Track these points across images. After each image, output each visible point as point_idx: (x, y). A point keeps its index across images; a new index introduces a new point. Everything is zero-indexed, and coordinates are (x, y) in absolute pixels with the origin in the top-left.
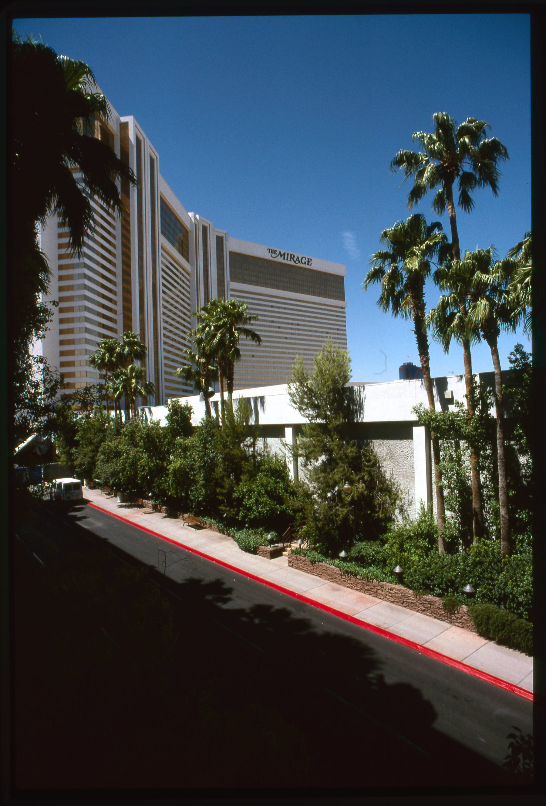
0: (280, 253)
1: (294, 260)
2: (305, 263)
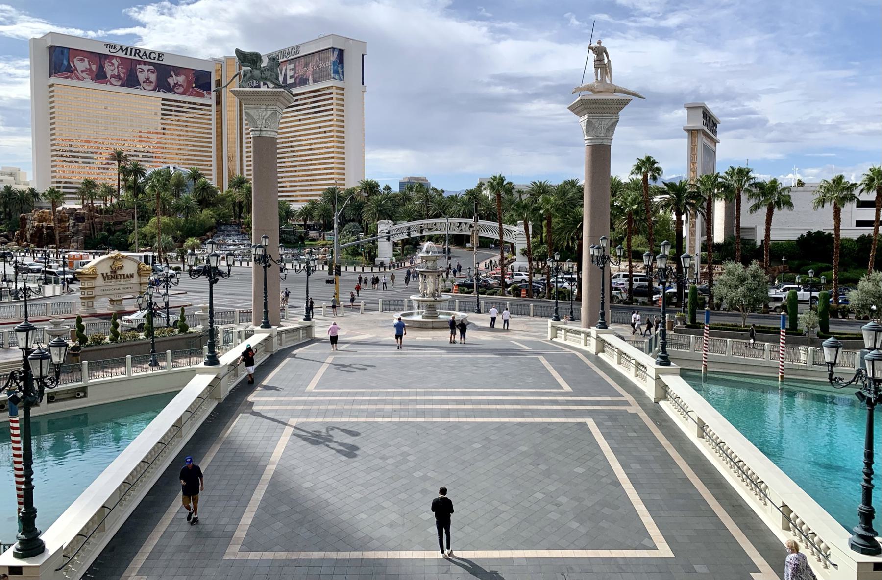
0: (121, 48)
1: (139, 56)
2: (154, 58)
